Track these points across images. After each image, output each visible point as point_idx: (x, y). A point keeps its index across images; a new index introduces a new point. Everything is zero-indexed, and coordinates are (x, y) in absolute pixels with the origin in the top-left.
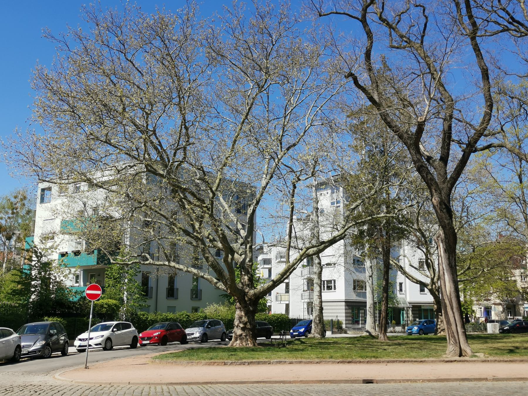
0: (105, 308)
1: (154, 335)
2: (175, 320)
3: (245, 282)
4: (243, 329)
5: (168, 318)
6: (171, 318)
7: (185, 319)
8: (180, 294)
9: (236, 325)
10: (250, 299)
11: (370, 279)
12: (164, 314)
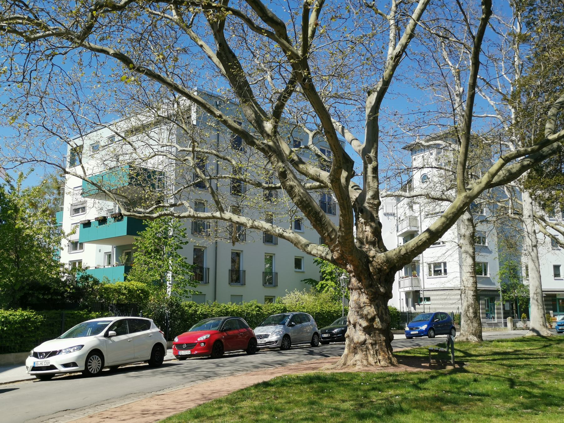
0: (124, 294)
1: (199, 339)
2: (239, 314)
3: (367, 238)
4: (368, 330)
5: (229, 310)
6: (233, 311)
7: (254, 313)
8: (249, 278)
9: (352, 322)
10: (380, 270)
11: (533, 250)
12: (223, 305)
